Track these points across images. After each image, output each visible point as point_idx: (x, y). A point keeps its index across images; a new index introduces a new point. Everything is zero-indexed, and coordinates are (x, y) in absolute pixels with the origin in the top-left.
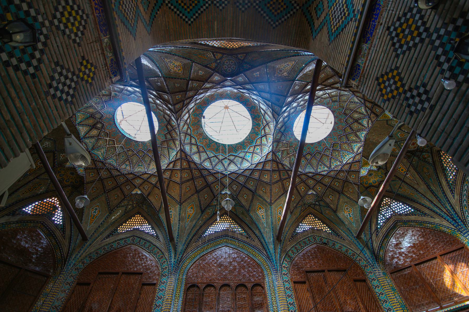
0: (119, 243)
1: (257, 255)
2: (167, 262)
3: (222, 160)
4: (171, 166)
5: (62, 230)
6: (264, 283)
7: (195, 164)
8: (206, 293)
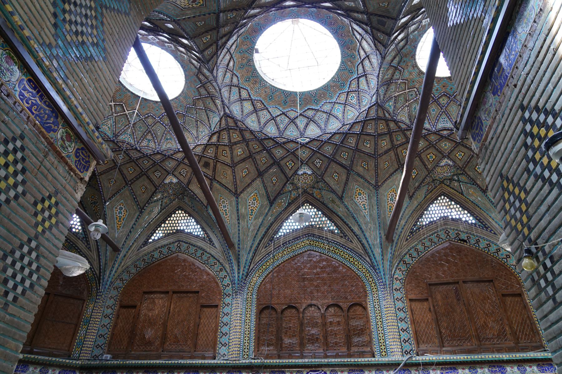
0: (162, 251)
1: (356, 263)
3: (295, 119)
4: (215, 139)
5: (85, 239)
6: (366, 302)
7: (252, 133)
8: (286, 317)
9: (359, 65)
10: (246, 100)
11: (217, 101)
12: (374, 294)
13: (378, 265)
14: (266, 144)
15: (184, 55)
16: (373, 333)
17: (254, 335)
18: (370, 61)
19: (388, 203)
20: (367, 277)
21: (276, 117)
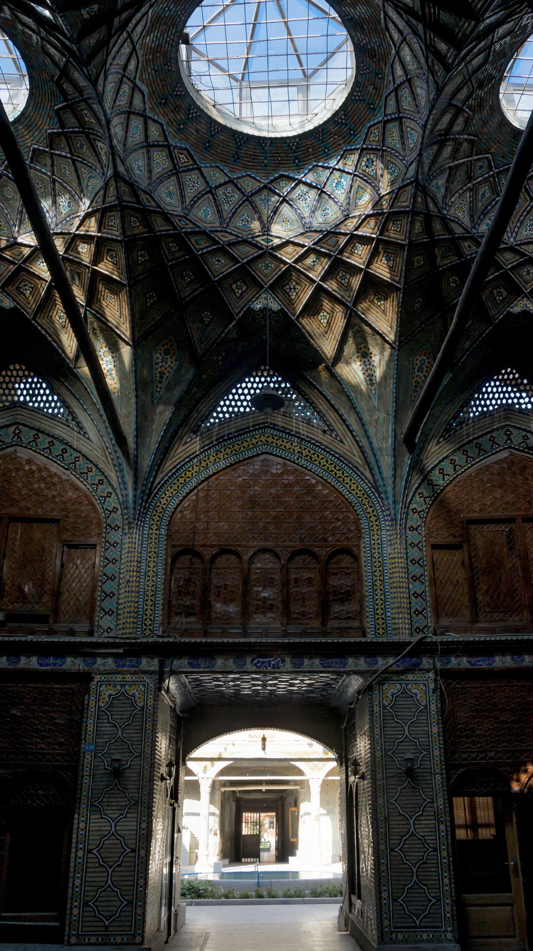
1: (347, 480)
2: (117, 495)
3: (253, 195)
8: (219, 568)
9: (389, 94)
10: (158, 146)
11: (99, 144)
12: (373, 535)
13: (384, 485)
14: (195, 243)
15: (31, 33)
16: (367, 599)
17: (162, 597)
18: (412, 92)
19: (414, 375)
20: (364, 505)
21: (217, 187)
